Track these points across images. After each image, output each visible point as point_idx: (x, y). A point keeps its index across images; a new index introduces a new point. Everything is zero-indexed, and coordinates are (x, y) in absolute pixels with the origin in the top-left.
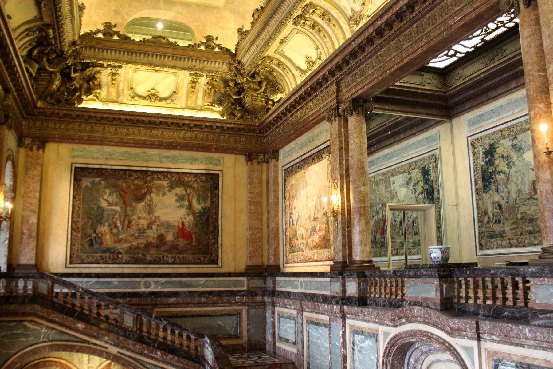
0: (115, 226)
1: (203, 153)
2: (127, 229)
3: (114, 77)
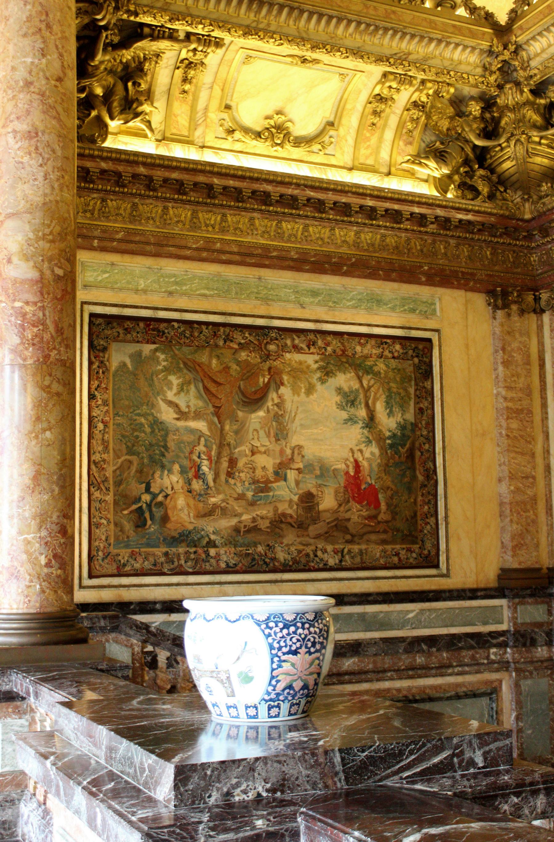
0: (199, 475)
1: (395, 285)
2: (227, 481)
3: (192, 73)
